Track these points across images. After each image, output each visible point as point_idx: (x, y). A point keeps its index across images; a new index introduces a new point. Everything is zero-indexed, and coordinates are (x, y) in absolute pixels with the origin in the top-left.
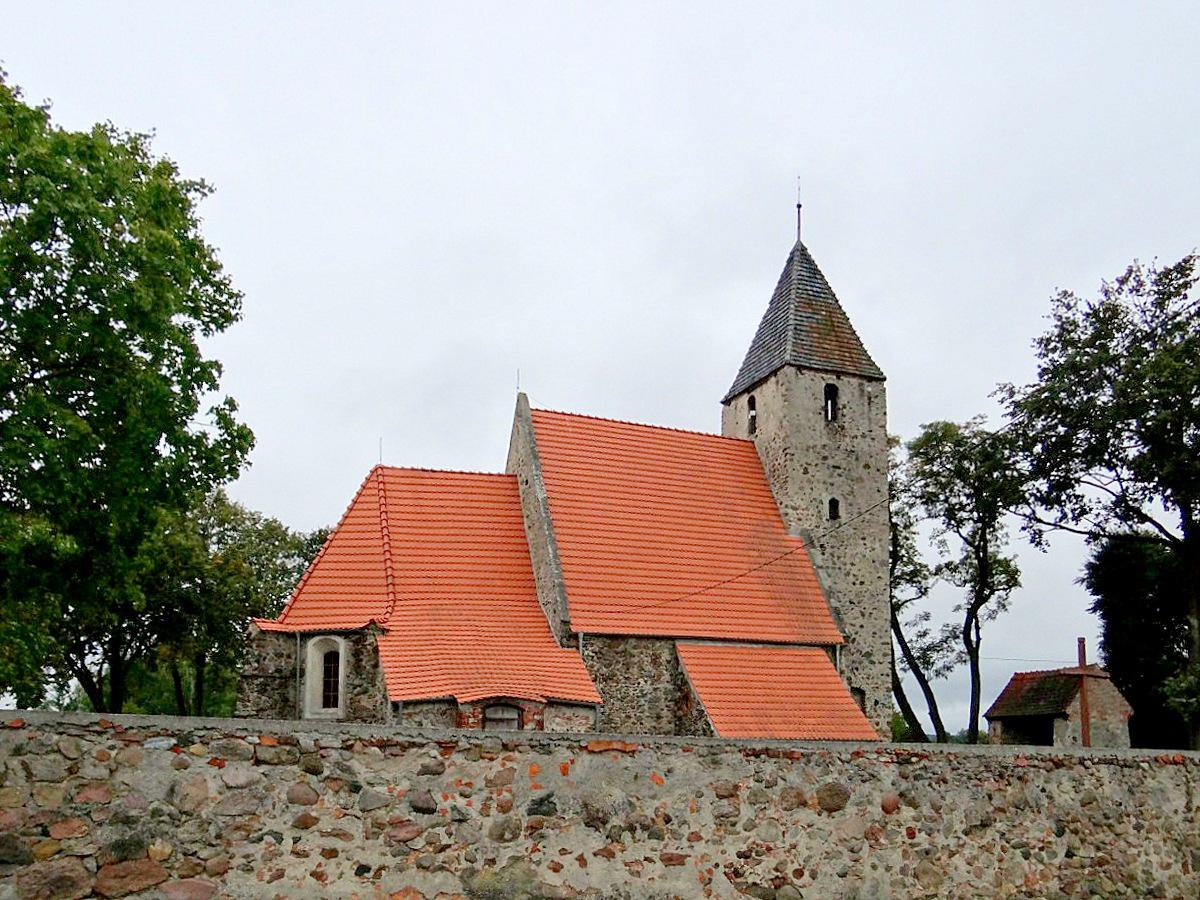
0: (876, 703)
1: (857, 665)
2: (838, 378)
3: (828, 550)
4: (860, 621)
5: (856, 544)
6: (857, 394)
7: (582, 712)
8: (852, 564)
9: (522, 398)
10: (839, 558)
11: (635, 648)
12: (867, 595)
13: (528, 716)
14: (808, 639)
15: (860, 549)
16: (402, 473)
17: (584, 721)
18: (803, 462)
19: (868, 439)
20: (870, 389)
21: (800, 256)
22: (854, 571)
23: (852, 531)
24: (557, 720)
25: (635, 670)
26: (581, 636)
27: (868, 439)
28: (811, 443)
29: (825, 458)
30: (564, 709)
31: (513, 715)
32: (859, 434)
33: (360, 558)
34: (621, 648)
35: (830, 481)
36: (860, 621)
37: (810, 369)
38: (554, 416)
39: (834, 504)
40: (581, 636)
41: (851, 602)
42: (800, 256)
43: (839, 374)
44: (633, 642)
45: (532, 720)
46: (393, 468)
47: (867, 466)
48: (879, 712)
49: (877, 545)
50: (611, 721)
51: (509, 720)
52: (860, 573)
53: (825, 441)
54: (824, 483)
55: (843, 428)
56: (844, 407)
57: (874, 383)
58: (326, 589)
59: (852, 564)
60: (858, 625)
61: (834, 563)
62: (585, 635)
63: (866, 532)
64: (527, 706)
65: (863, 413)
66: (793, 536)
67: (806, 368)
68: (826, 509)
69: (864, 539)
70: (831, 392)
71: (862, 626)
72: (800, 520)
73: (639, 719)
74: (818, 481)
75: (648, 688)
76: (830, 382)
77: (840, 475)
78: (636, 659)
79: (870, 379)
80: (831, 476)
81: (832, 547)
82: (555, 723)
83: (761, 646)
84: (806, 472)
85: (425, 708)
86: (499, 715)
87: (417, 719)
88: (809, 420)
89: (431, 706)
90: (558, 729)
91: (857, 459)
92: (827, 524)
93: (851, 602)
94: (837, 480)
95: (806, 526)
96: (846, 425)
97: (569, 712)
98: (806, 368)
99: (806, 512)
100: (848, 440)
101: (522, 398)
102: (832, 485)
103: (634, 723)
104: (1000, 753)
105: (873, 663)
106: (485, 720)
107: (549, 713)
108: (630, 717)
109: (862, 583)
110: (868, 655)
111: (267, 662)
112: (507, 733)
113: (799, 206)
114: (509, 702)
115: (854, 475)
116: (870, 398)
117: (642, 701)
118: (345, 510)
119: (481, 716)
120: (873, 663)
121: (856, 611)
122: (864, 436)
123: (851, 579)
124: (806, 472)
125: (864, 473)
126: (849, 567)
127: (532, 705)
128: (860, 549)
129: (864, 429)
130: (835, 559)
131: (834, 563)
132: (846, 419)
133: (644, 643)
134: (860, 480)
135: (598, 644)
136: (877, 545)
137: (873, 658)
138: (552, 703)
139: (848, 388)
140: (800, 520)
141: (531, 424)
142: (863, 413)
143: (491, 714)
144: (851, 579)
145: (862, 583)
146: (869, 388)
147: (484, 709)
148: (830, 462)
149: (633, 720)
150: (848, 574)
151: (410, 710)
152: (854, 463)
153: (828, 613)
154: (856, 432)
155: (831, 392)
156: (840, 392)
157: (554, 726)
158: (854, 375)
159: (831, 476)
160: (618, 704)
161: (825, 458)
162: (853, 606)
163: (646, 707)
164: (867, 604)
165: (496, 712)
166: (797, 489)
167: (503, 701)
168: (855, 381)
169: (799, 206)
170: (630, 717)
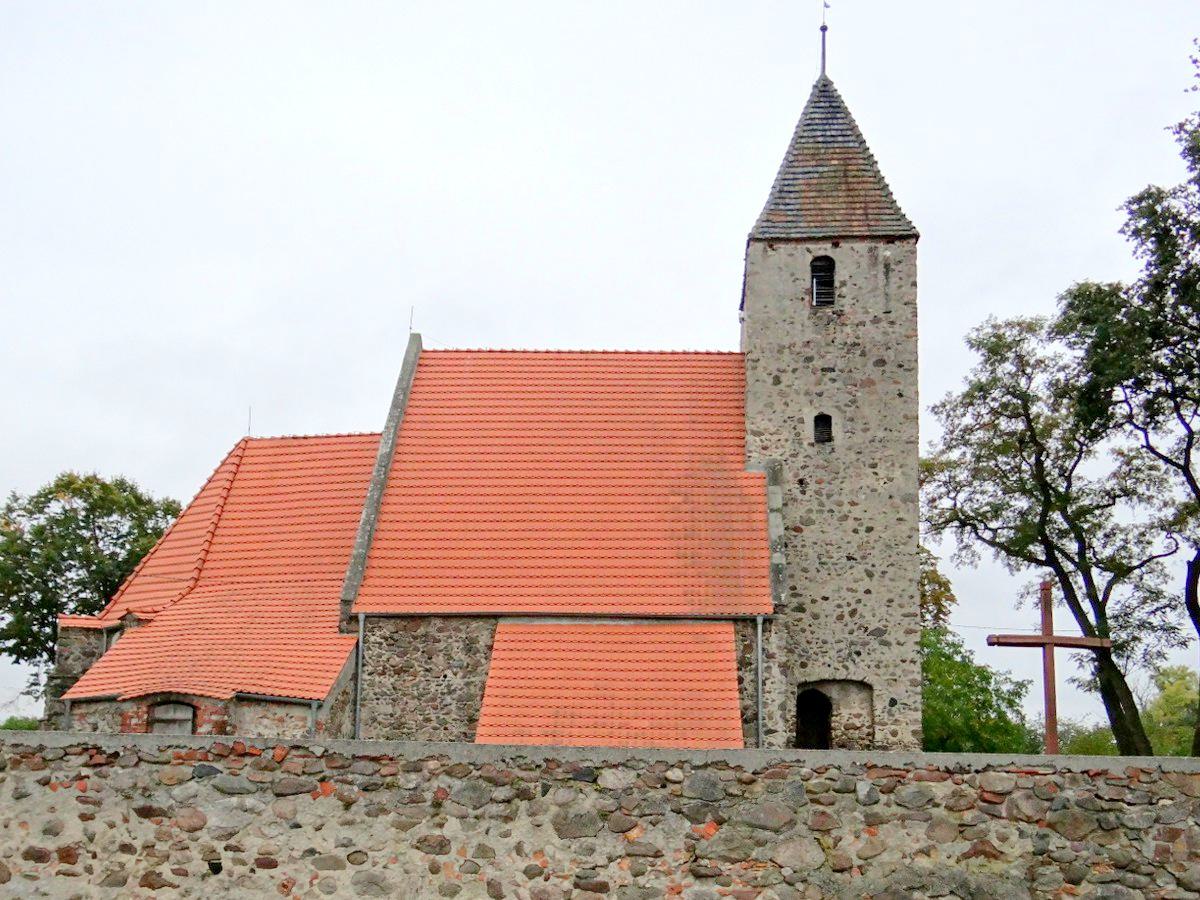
0: (893, 702)
1: (858, 648)
2: (836, 245)
3: (812, 487)
4: (866, 583)
5: (859, 475)
6: (865, 262)
7: (297, 712)
8: (853, 504)
9: (416, 339)
10: (829, 496)
11: (440, 630)
12: (879, 546)
13: (203, 716)
14: (709, 611)
15: (870, 481)
16: (272, 444)
17: (301, 724)
18: (773, 368)
19: (884, 324)
20: (888, 253)
21: (825, 98)
22: (857, 512)
23: (853, 456)
24: (265, 721)
25: (440, 659)
26: (361, 617)
27: (884, 324)
28: (786, 342)
29: (809, 359)
30: (275, 709)
31: (187, 714)
32: (868, 319)
33: (534, 553)
34: (421, 630)
35: (818, 389)
36: (866, 583)
37: (788, 240)
38: (570, 356)
39: (823, 422)
40: (361, 617)
41: (849, 558)
42: (825, 98)
43: (835, 242)
44: (438, 623)
45: (209, 721)
46: (262, 440)
47: (881, 362)
48: (897, 716)
49: (897, 473)
50: (401, 726)
51: (181, 722)
52: (868, 515)
53: (809, 335)
54: (807, 393)
55: (840, 314)
56: (843, 284)
57: (897, 243)
58: (614, 590)
59: (853, 504)
60: (862, 589)
61: (821, 504)
62: (367, 617)
63: (878, 455)
64: (203, 705)
65: (876, 289)
66: (753, 472)
67: (779, 240)
68: (809, 431)
69: (874, 466)
70: (823, 270)
71: (868, 592)
72: (765, 448)
73: (444, 724)
74: (797, 393)
75: (457, 681)
76: (822, 253)
77: (834, 380)
78: (442, 645)
79: (890, 239)
80: (818, 383)
81: (819, 482)
82: (256, 726)
83: (632, 622)
84: (777, 381)
85: (100, 707)
86: (170, 715)
87: (92, 720)
88: (783, 311)
89: (107, 705)
90: (266, 733)
91: (863, 354)
92: (811, 451)
93: (849, 558)
94: (828, 386)
95: (776, 456)
96: (847, 309)
97: (281, 711)
98: (779, 240)
99: (776, 437)
100: (848, 329)
101: (416, 339)
102: (820, 395)
103: (435, 729)
104: (433, 748)
105: (887, 644)
106: (150, 724)
107: (249, 713)
108: (428, 720)
109: (869, 530)
110: (879, 633)
111: (70, 661)
112: (179, 736)
113: (824, 29)
114: (181, 698)
115: (858, 376)
116: (887, 266)
117: (448, 699)
118: (197, 490)
119: (145, 717)
120: (887, 644)
121: (859, 570)
122: (876, 320)
123: (850, 524)
124: (777, 381)
125: (875, 373)
126: (846, 508)
127: (208, 703)
128: (870, 481)
129: (877, 310)
130: (824, 499)
131: (821, 504)
132: (847, 302)
133: (454, 623)
134: (870, 383)
135: (388, 628)
136: (897, 473)
137: (886, 637)
138: (242, 699)
139: (849, 261)
140: (765, 448)
141: (422, 368)
142: (876, 289)
143: (161, 713)
144: (850, 524)
145: (869, 530)
146: (886, 251)
147: (151, 707)
148: (818, 363)
149: (434, 724)
150: (845, 517)
151: (83, 709)
152: (858, 359)
153: (765, 572)
154: (861, 317)
155: (823, 270)
156: (837, 265)
157: (261, 730)
158: (863, 238)
159: (818, 383)
160: (413, 704)
161: (809, 359)
162: (853, 562)
163: (453, 707)
164: (877, 559)
165: (167, 711)
166: (760, 407)
167: (173, 698)
168: (862, 247)
169: (824, 29)
170: (428, 720)
